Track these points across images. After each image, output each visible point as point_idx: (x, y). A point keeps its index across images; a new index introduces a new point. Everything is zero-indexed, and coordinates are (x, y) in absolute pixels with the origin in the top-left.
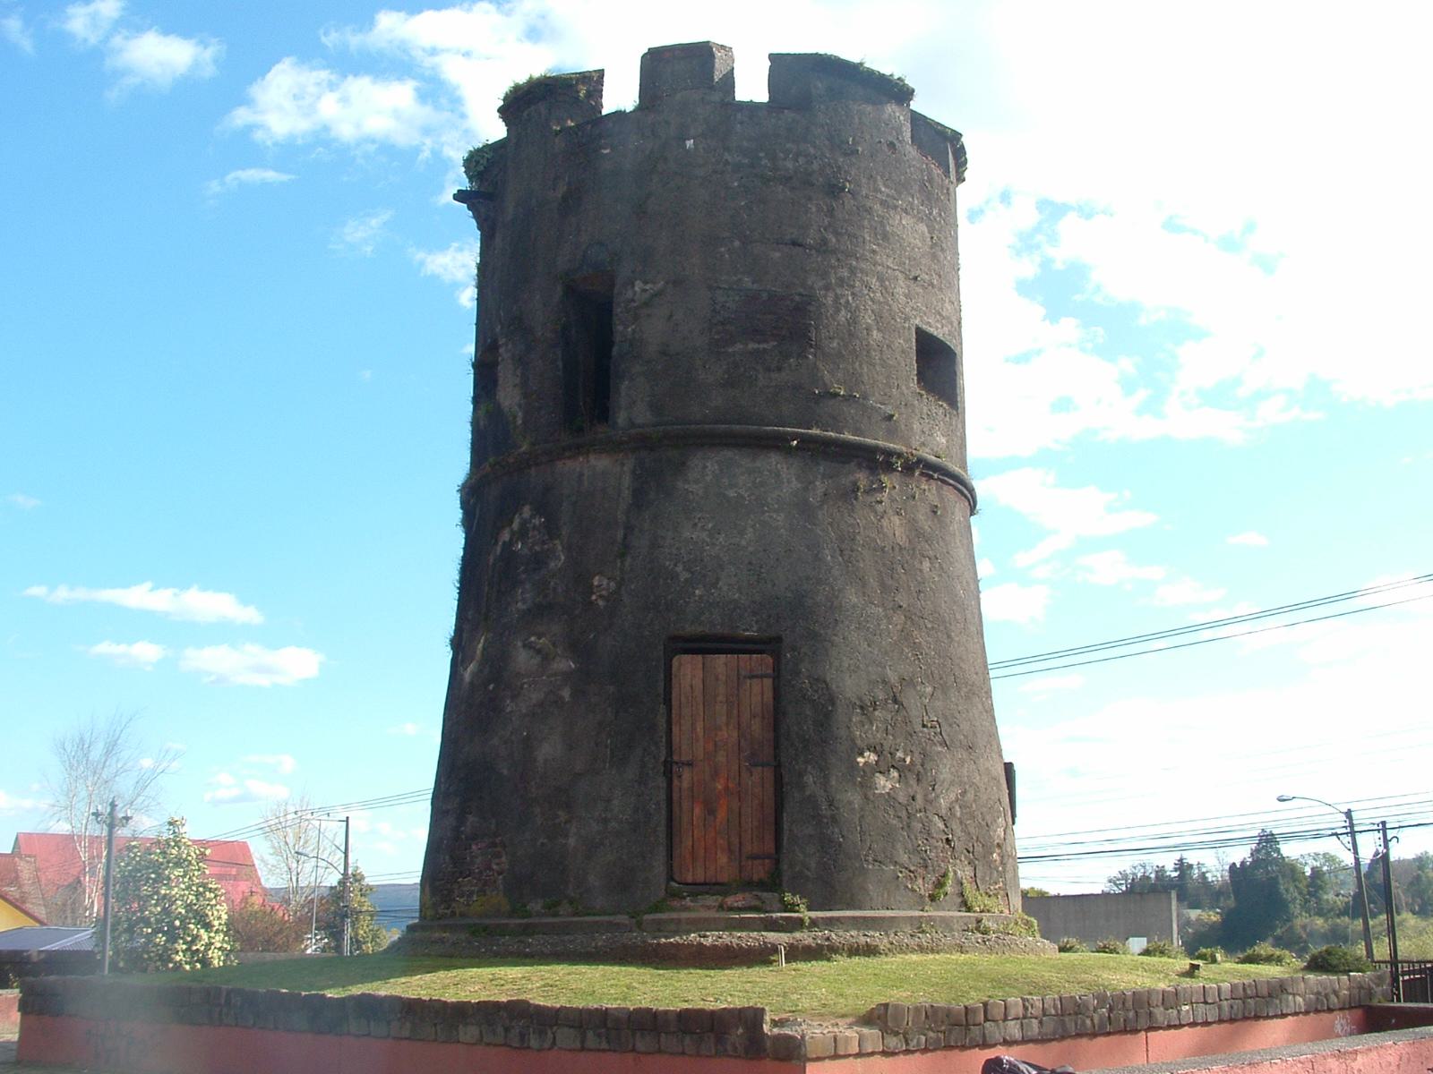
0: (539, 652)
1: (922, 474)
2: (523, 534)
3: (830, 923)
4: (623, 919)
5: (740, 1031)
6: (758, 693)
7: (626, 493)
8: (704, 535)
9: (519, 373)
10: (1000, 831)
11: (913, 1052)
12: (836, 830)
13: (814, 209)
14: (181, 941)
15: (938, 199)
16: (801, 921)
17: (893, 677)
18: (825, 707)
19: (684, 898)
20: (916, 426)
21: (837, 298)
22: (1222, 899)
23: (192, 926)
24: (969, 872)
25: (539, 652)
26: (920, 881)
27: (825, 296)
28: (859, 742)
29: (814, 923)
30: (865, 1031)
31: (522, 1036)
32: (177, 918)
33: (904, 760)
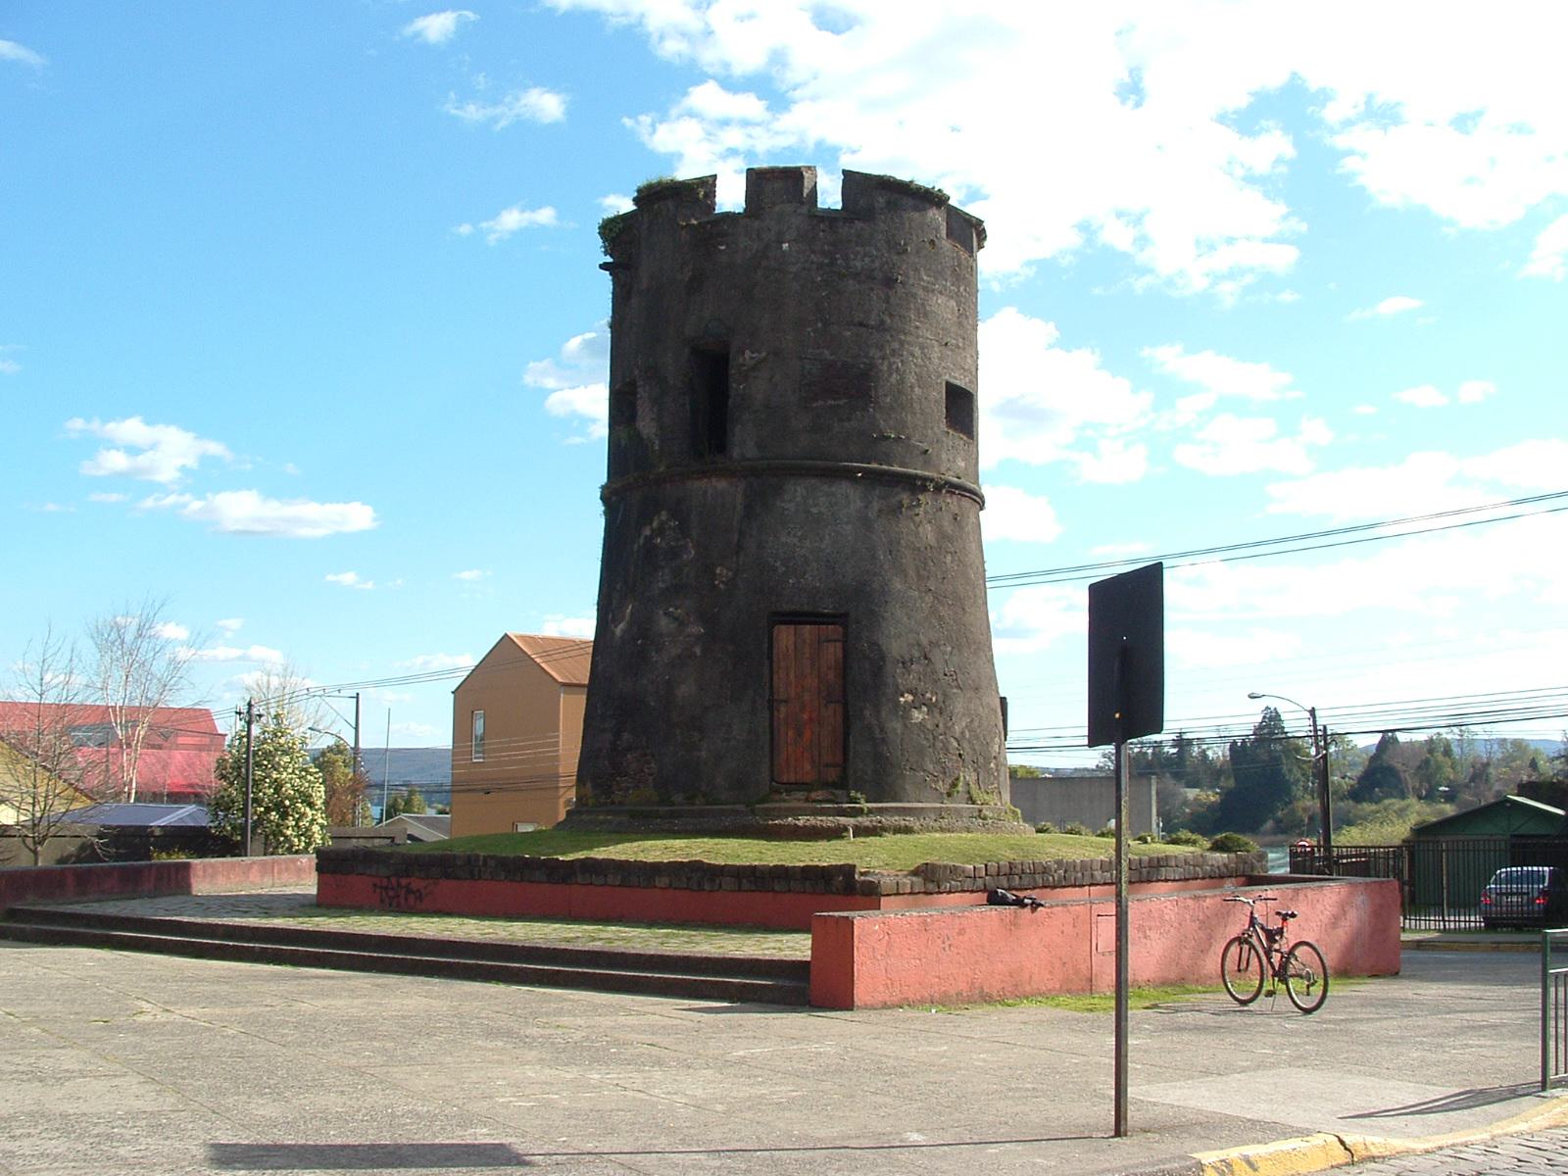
0: (676, 619)
1: (948, 492)
2: (660, 531)
3: (880, 811)
4: (741, 807)
5: (841, 878)
6: (833, 652)
7: (739, 507)
8: (796, 540)
9: (655, 410)
10: (996, 748)
11: (942, 893)
12: (885, 748)
13: (875, 297)
14: (291, 818)
15: (965, 278)
16: (862, 810)
17: (924, 641)
18: (878, 663)
19: (781, 793)
20: (944, 456)
21: (890, 365)
22: (1223, 779)
23: (299, 805)
24: (974, 776)
25: (676, 619)
26: (941, 783)
27: (882, 364)
28: (901, 687)
29: (870, 811)
30: (914, 879)
31: (699, 884)
32: (287, 798)
33: (931, 699)
